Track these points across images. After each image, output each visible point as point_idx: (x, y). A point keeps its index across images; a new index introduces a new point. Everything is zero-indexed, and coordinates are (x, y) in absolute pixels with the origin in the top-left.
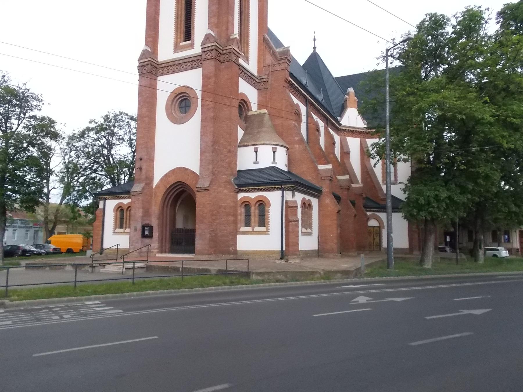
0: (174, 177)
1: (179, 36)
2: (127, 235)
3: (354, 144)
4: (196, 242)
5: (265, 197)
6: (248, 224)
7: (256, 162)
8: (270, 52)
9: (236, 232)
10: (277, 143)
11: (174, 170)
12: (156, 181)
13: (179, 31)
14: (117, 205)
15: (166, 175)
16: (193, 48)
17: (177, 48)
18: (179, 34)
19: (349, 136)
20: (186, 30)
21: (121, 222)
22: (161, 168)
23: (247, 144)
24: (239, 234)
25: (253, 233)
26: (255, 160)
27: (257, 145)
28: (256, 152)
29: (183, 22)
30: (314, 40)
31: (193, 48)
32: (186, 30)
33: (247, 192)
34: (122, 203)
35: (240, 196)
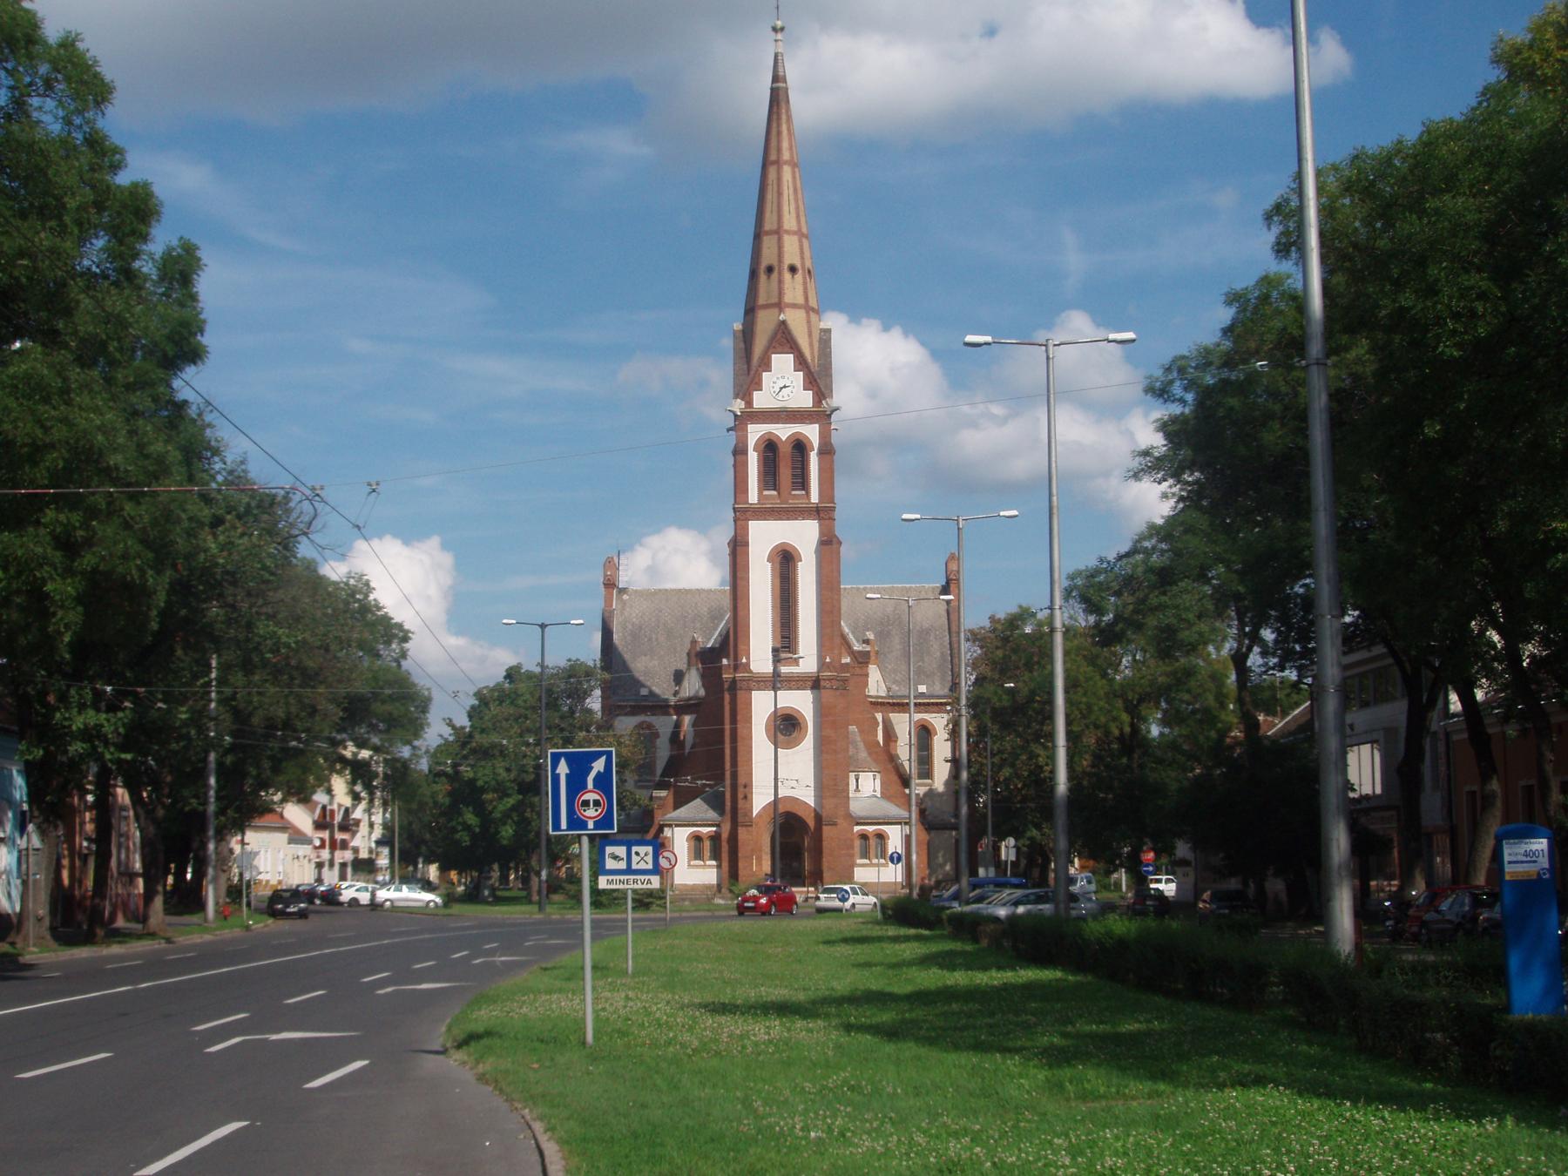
6: (865, 854)
9: (853, 865)
21: (697, 854)
25: (871, 865)
35: (857, 828)
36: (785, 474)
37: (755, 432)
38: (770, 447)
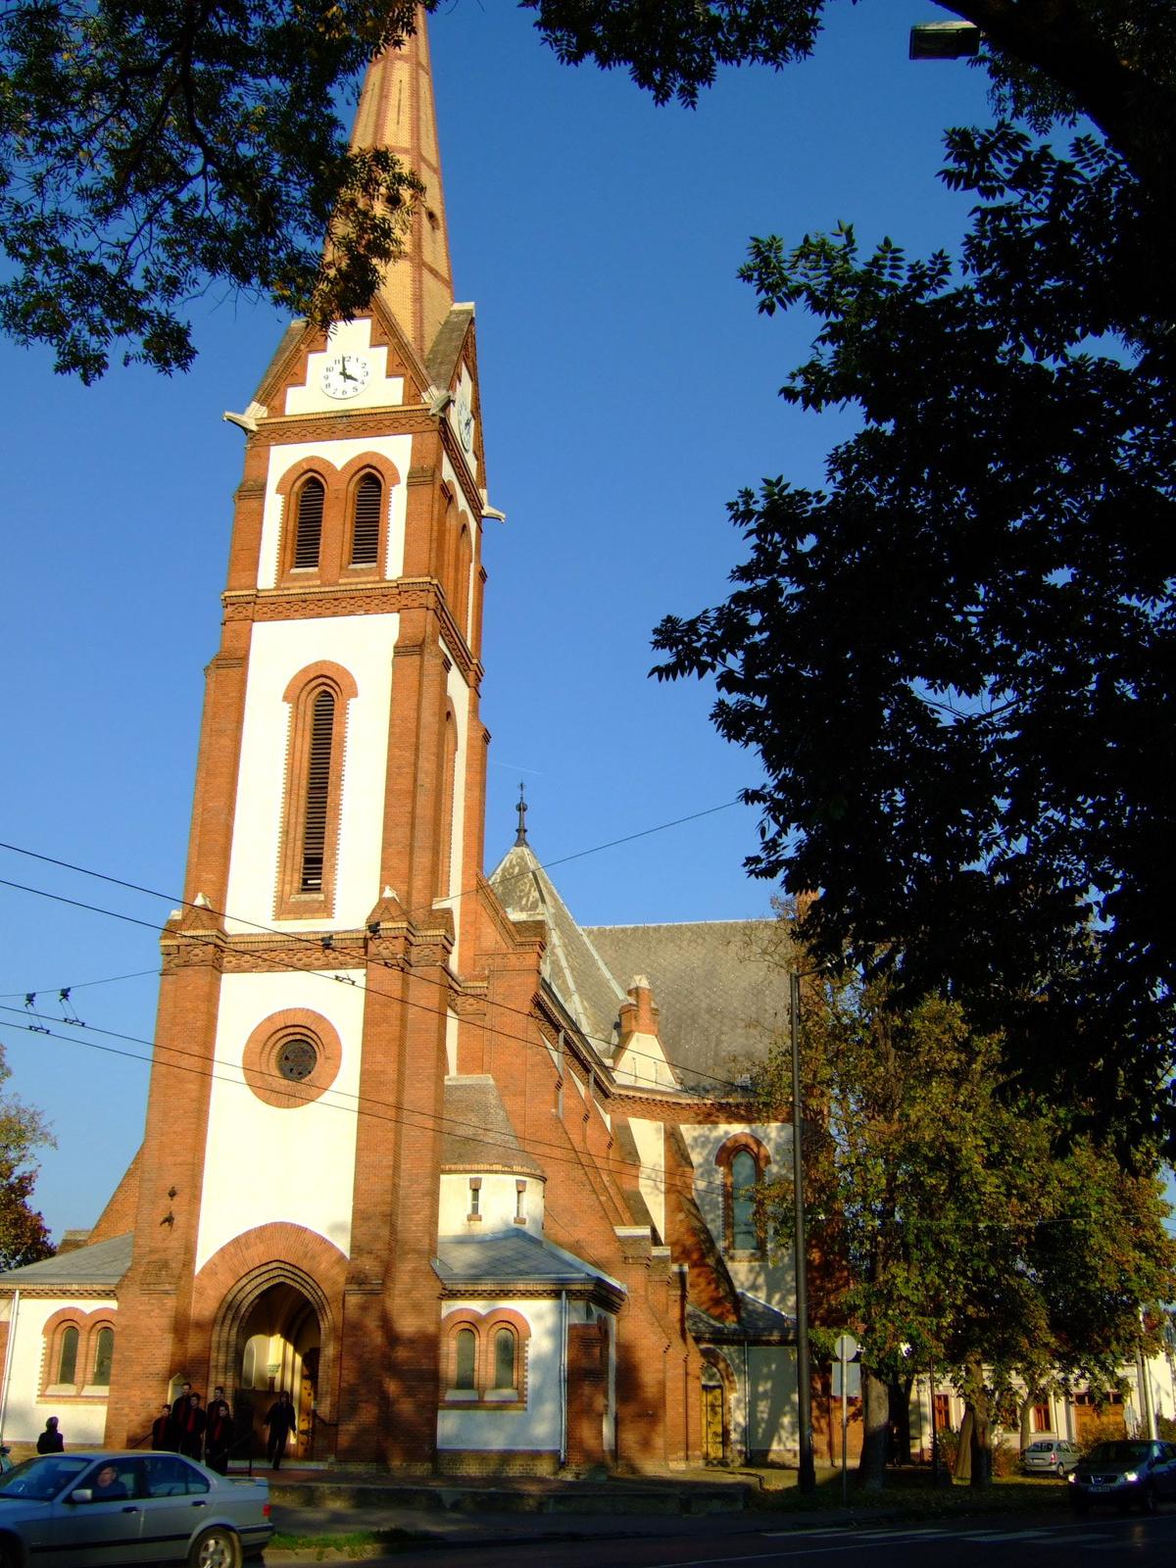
0: (261, 1248)
1: (288, 878)
2: (102, 1403)
3: (648, 1138)
4: (862, 1442)
5: (516, 1314)
7: (475, 1214)
8: (493, 922)
10: (526, 1170)
11: (263, 1229)
12: (203, 1257)
13: (289, 866)
14: (57, 1314)
15: (236, 1241)
16: (330, 915)
17: (283, 909)
18: (288, 872)
19: (635, 1116)
20: (311, 862)
22: (223, 1220)
23: (453, 1167)
24: (443, 1408)
26: (469, 1210)
27: (478, 1172)
28: (476, 1191)
29: (299, 843)
30: (521, 808)
31: (330, 915)
32: (311, 862)
33: (467, 1299)
34: (75, 1310)
36: (337, 528)
37: (283, 459)
38: (310, 489)
